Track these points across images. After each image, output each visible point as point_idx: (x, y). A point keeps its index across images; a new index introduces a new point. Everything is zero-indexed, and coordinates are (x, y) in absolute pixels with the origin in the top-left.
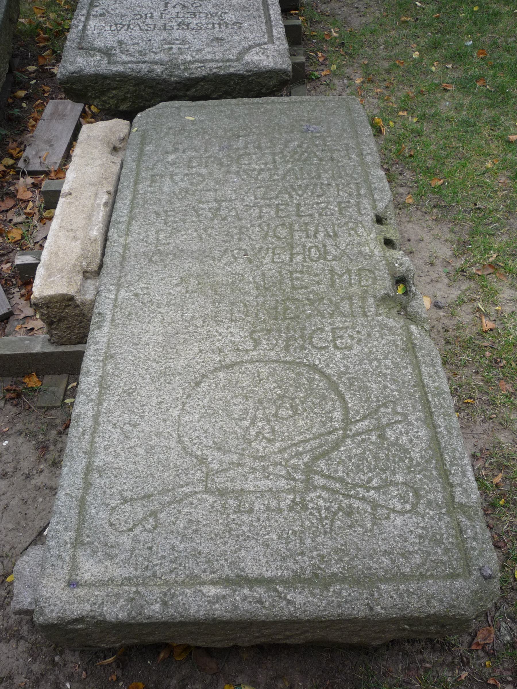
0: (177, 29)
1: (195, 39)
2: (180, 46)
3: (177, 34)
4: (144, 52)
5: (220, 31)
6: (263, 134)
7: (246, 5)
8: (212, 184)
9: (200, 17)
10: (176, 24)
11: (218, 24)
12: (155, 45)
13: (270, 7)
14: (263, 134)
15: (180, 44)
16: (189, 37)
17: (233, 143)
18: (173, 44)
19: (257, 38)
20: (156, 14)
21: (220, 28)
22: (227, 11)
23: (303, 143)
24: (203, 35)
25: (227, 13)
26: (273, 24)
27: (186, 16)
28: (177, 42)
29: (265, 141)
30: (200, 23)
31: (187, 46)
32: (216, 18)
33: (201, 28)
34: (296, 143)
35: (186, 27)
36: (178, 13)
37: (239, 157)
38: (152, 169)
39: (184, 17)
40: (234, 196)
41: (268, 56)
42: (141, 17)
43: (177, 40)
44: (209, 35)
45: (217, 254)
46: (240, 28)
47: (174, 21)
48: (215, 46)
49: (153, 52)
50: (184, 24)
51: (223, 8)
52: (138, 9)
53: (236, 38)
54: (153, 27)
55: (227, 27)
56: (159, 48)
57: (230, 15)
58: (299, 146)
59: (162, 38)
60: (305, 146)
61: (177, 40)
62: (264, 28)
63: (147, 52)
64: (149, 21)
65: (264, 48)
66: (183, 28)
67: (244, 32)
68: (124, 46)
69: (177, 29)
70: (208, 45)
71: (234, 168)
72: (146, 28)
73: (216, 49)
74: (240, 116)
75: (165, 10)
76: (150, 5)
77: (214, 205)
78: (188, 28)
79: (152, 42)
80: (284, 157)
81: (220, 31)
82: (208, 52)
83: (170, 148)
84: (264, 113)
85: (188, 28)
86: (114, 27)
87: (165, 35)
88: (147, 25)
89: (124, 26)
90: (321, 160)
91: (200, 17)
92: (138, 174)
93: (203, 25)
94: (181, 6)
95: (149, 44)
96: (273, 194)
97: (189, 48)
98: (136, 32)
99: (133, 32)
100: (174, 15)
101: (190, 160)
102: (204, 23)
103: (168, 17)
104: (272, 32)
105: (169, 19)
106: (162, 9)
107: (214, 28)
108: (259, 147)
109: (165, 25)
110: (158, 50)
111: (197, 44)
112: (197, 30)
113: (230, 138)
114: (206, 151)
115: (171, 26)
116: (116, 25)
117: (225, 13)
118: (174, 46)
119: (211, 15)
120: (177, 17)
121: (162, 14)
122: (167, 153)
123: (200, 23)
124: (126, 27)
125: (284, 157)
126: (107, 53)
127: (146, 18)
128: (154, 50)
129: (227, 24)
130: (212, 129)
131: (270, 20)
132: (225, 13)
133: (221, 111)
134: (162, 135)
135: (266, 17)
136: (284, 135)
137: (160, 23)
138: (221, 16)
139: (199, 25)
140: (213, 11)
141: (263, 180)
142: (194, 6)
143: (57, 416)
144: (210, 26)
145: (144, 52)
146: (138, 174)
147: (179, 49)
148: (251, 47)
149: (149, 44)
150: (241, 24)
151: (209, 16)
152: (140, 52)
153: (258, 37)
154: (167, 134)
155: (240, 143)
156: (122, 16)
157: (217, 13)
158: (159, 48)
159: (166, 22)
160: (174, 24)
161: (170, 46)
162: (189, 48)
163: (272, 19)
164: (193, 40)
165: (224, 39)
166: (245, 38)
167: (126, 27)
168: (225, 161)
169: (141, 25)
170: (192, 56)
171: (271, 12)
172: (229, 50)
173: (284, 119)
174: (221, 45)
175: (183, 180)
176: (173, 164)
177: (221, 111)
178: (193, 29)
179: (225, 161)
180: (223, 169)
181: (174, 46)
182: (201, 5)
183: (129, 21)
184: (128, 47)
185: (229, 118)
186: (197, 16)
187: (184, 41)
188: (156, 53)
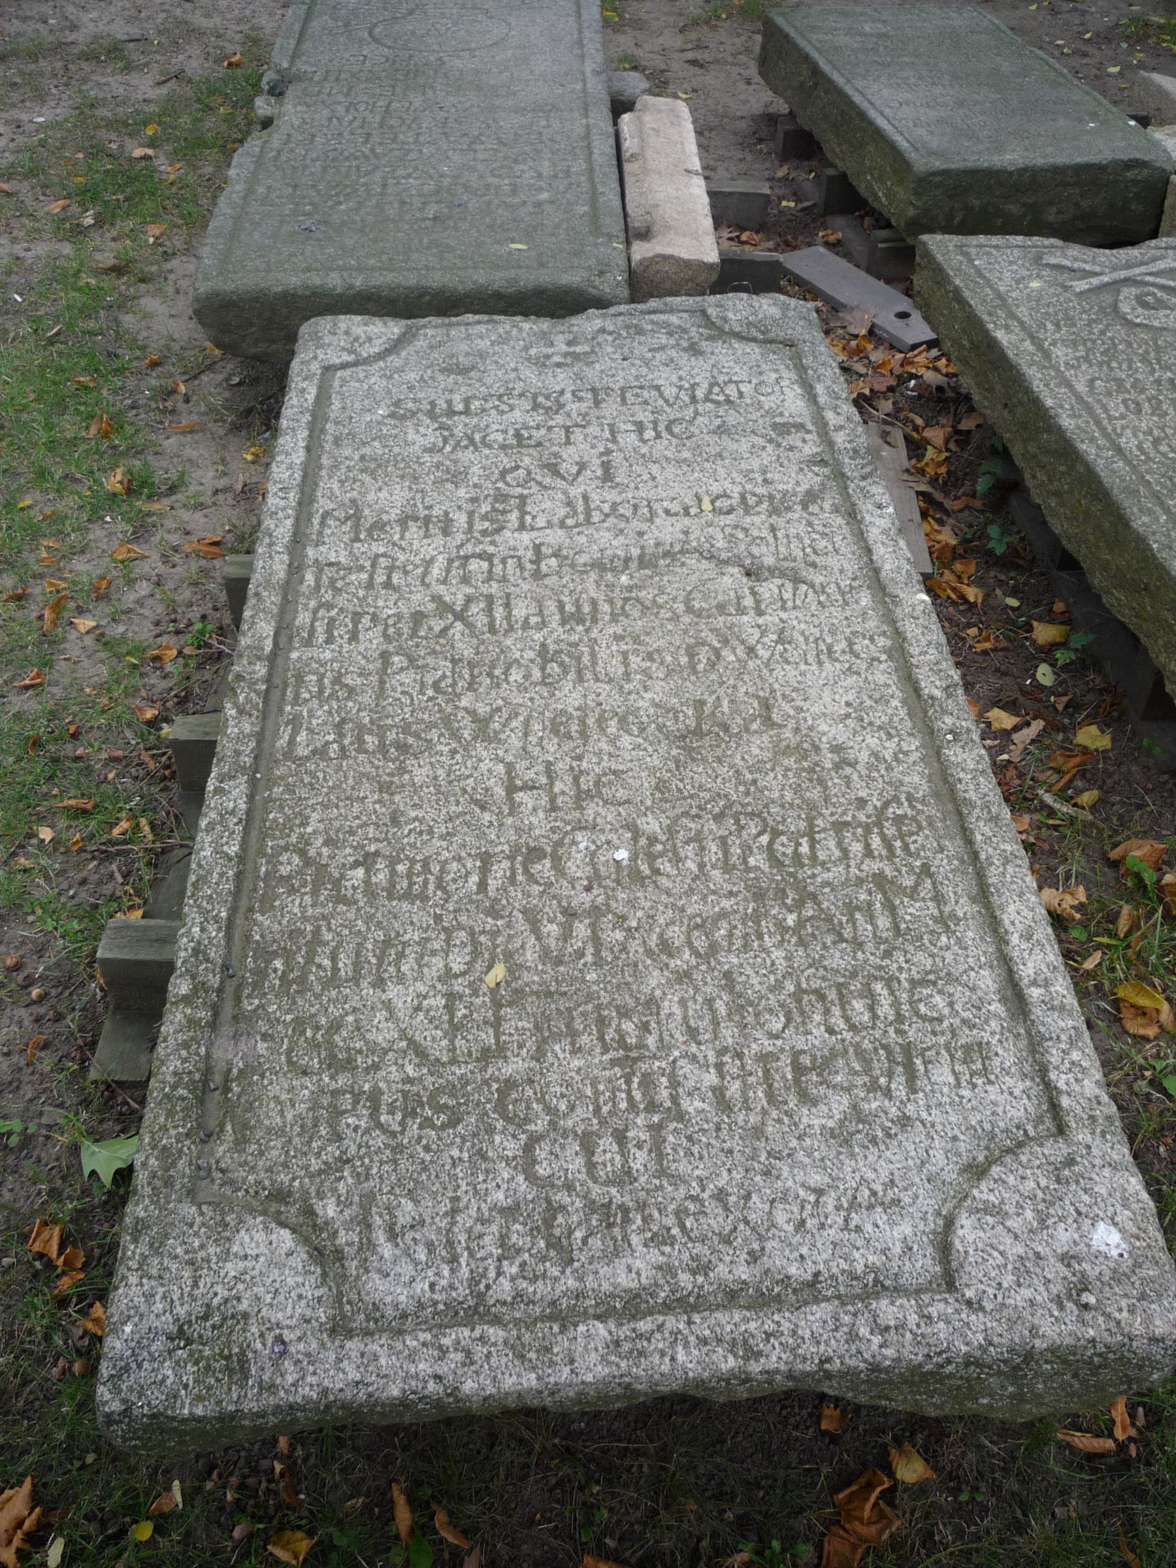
0: (562, 392)
1: (516, 370)
2: (550, 351)
3: (561, 380)
4: (632, 331)
5: (451, 391)
6: (393, 221)
7: (367, 479)
8: (480, 166)
9: (505, 432)
10: (568, 408)
11: (455, 413)
12: (609, 349)
13: (298, 476)
14: (393, 221)
15: (548, 357)
16: (529, 374)
17: (446, 210)
18: (566, 355)
19: (362, 375)
20: (629, 439)
21: (449, 402)
22: (427, 457)
23: (331, 208)
24: (494, 378)
25: (426, 450)
26: (307, 417)
27: (543, 431)
28: (557, 359)
29: (391, 212)
30: (503, 412)
31: (533, 352)
32: (459, 431)
33: (500, 397)
34: (342, 207)
35: (540, 399)
36: (568, 442)
37: (437, 192)
38: (571, 184)
39: (550, 429)
40: (450, 153)
41: (347, 333)
42: (668, 429)
43: (559, 365)
44: (480, 380)
45: (475, 110)
46: (397, 403)
47: (574, 415)
48: (467, 354)
49: (610, 333)
50: (548, 410)
51: (437, 466)
52: (686, 454)
53: (412, 376)
54: (628, 395)
55: (433, 404)
56: (599, 344)
57: (420, 441)
58: (340, 203)
59: (597, 366)
60: (330, 203)
61: (559, 365)
62: (336, 404)
63: (624, 333)
64: (645, 416)
65: (350, 352)
66: (547, 397)
67: (389, 392)
68: (685, 344)
69: (562, 392)
70: (482, 355)
71: (446, 182)
72: (646, 394)
73: (464, 347)
74: (428, 248)
75: (608, 452)
76: (655, 469)
77: (478, 147)
78: (535, 396)
79: (618, 356)
80: (368, 191)
81: (451, 391)
82: (482, 337)
83: (548, 208)
84: (383, 252)
85: (535, 396)
86: (731, 390)
87: (592, 374)
88: (646, 403)
89: (707, 399)
90: (314, 186)
91: (505, 432)
92: (591, 180)
93: (496, 407)
94: (563, 468)
95: (626, 350)
96: (397, 153)
97: (526, 349)
98: (665, 377)
99: (674, 378)
100: (578, 435)
101: (514, 192)
102: (493, 412)
103: (593, 430)
104: (318, 399)
105: (589, 423)
106: (617, 458)
107: (467, 401)
108: (403, 203)
109: (597, 403)
110: (600, 339)
111: (510, 357)
112: (509, 392)
113: (449, 218)
114: (489, 203)
115: (580, 399)
116: (728, 401)
117: (430, 450)
118: (564, 348)
119: (472, 441)
120: (567, 430)
121: (614, 440)
122: (553, 202)
123: (503, 412)
124: (700, 393)
125: (368, 191)
126: (720, 332)
127: (655, 423)
128: (610, 338)
129: (431, 414)
130: (479, 231)
131: (311, 431)
132: (430, 450)
133: (461, 257)
134: (565, 226)
135: (323, 431)
136: (357, 218)
137: (610, 408)
138: (445, 441)
139: (506, 408)
140: (467, 456)
141: (405, 168)
142: (521, 473)
143: (1148, 1126)
144: (475, 405)
145: (632, 331)
146: (591, 180)
147: (552, 344)
148: (381, 356)
149: (626, 350)
150: (392, 415)
151: (477, 437)
152: (640, 332)
153: (359, 380)
154: (557, 226)
155: (431, 211)
156: (721, 430)
157: (454, 449)
158: (599, 344)
159: (596, 412)
160: (573, 407)
161: (572, 349)
162: (526, 349)
163: (306, 433)
164: (520, 366)
165: (442, 371)
166: (391, 377)
167: (700, 393)
168: (460, 190)
169: (661, 402)
170: (521, 330)
171: (299, 457)
172: (431, 347)
173: (349, 242)
174: (452, 356)
175: (523, 172)
176: (541, 189)
177: (461, 257)
178: (521, 395)
179: (460, 190)
180: (463, 181)
181: (564, 348)
182: (503, 474)
183: (697, 413)
184: (672, 342)
185: (448, 246)
186: (511, 432)
187: (541, 363)
188: (602, 331)
